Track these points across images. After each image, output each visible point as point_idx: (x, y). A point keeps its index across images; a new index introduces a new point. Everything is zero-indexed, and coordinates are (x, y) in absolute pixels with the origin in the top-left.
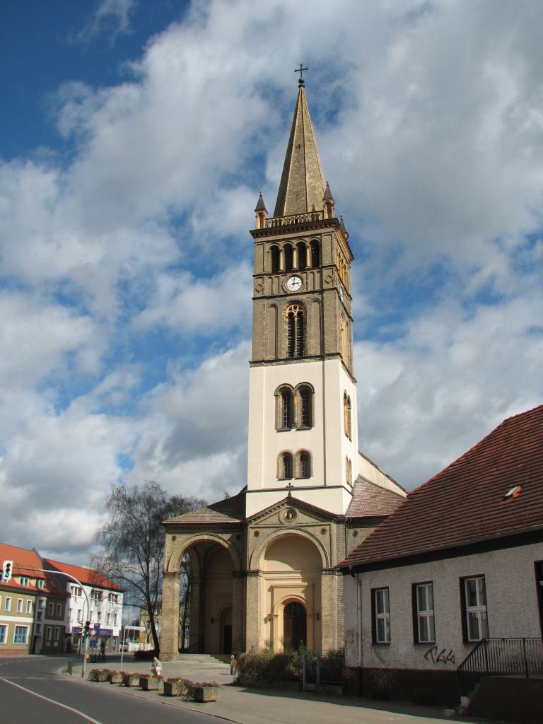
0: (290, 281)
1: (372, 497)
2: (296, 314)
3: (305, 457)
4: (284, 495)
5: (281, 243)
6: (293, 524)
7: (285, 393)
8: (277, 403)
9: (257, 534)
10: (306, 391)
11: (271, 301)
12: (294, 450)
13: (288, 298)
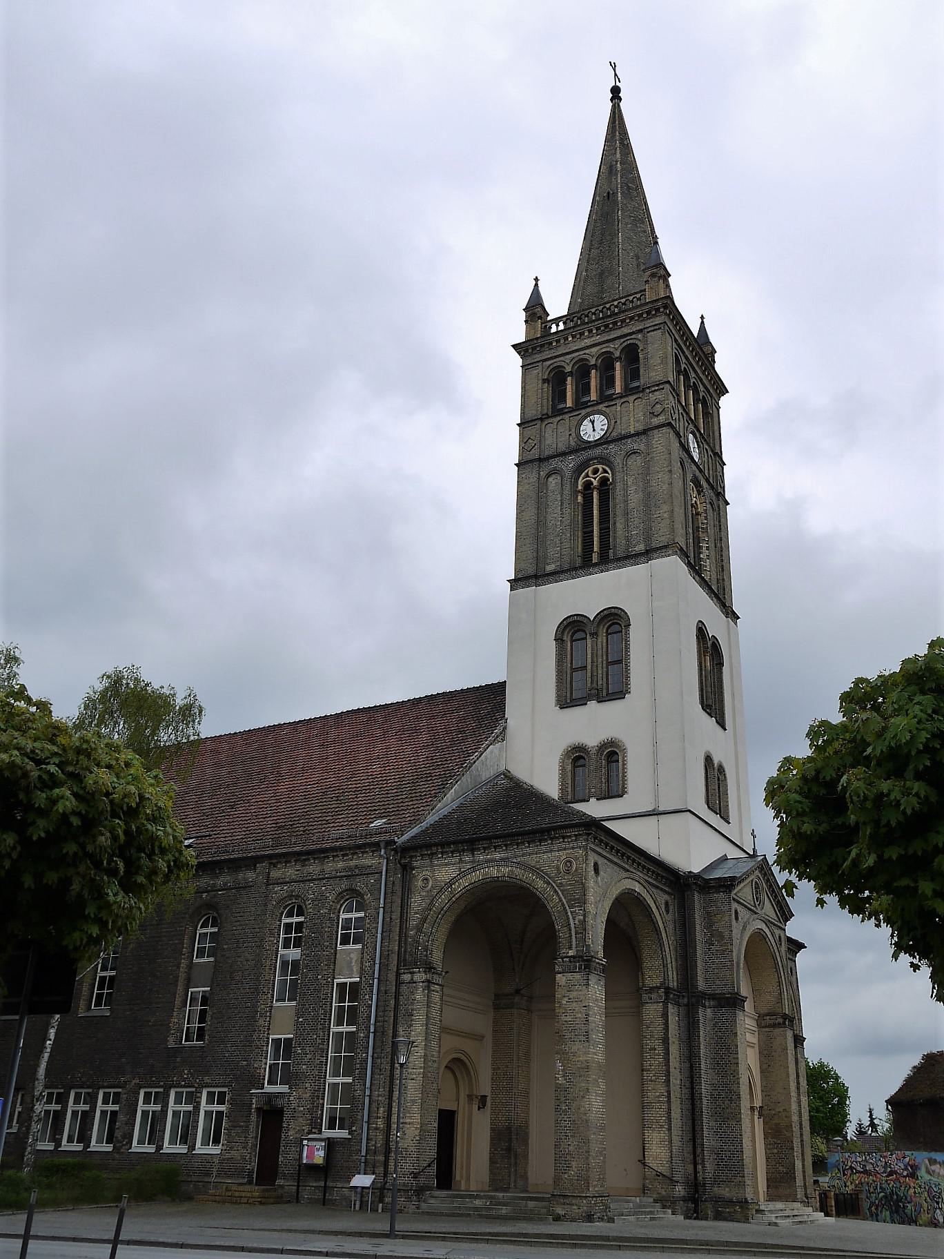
3: (612, 753)
7: (573, 628)
10: (614, 620)
12: (592, 741)
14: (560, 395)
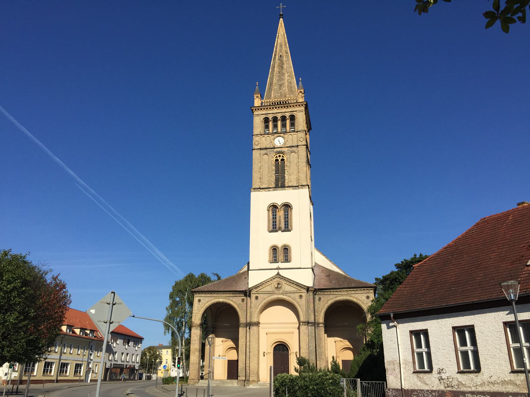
0: (277, 140)
1: (327, 276)
2: (280, 160)
3: (286, 249)
4: (276, 272)
5: (287, 114)
6: (281, 291)
7: (274, 207)
8: (269, 215)
9: (257, 298)
10: (287, 206)
11: (264, 152)
12: (280, 245)
13: (275, 150)
14: (267, 127)
